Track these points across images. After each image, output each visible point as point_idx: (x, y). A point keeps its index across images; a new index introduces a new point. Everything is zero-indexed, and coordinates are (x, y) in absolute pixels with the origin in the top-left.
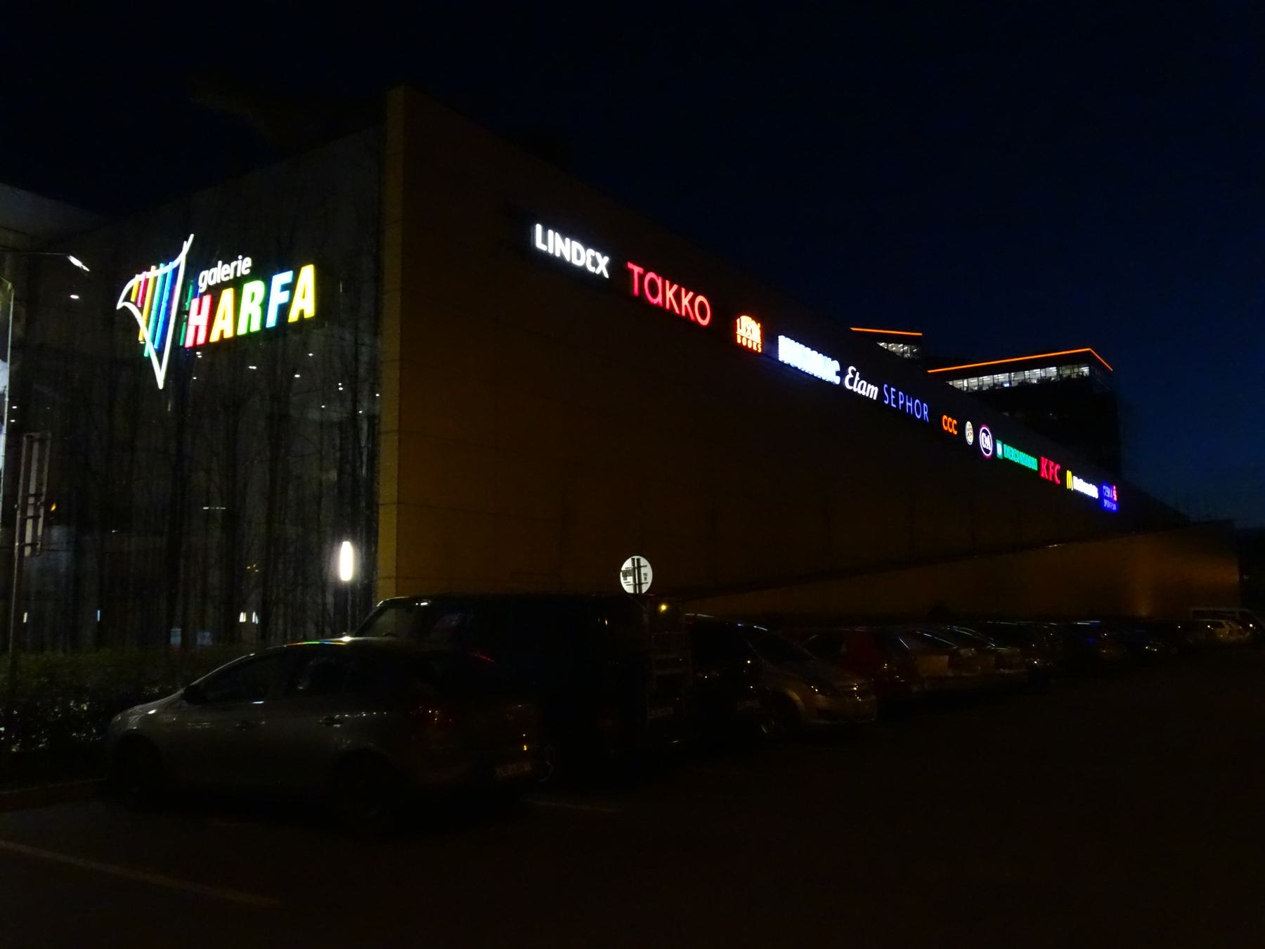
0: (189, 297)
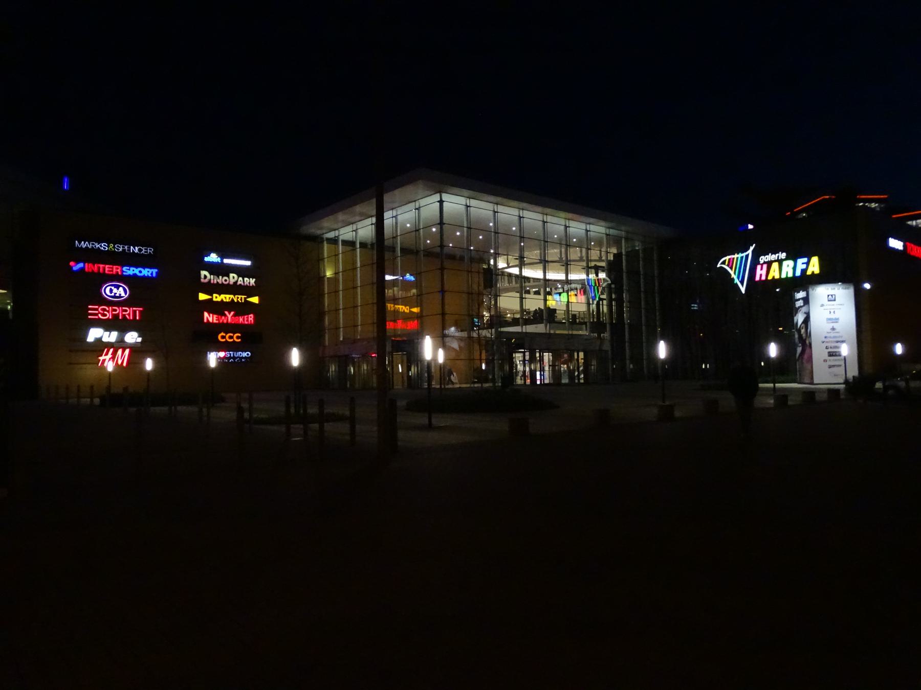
0: (104, 354)
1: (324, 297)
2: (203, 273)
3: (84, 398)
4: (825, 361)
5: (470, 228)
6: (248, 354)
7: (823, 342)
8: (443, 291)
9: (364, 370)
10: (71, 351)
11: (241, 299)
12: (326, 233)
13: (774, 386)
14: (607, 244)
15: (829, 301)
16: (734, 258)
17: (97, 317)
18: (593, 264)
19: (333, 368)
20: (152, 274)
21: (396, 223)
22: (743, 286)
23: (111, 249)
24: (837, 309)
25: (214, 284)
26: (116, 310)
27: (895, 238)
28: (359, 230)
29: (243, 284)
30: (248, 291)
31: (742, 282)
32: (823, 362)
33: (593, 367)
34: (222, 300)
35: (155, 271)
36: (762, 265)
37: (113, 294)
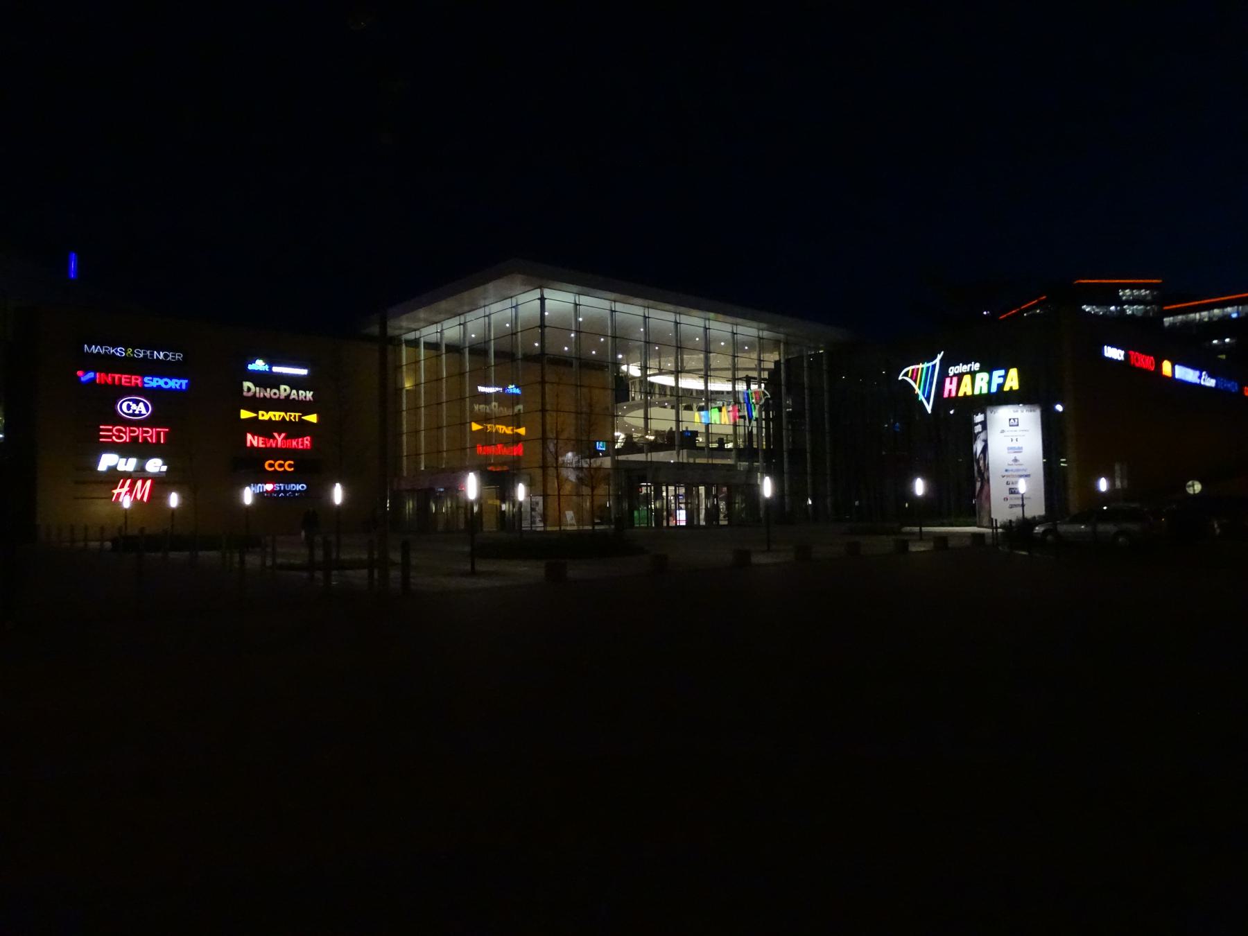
1: (401, 416)
2: (247, 384)
3: (92, 540)
4: (1006, 499)
5: (580, 332)
6: (303, 487)
7: (1003, 477)
8: (543, 411)
9: (447, 507)
10: (77, 482)
11: (295, 418)
12: (404, 334)
13: (921, 529)
14: (760, 347)
15: (1010, 426)
16: (918, 369)
17: (110, 440)
18: (741, 374)
19: (410, 505)
20: (181, 385)
21: (489, 324)
22: (928, 402)
23: (129, 355)
24: (1020, 436)
25: (260, 398)
26: (134, 432)
27: (1112, 346)
28: (519, 306)
29: (297, 398)
30: (304, 407)
31: (928, 399)
32: (1003, 501)
33: (737, 505)
34: (270, 419)
35: (184, 382)
36: (951, 377)
37: (131, 412)
